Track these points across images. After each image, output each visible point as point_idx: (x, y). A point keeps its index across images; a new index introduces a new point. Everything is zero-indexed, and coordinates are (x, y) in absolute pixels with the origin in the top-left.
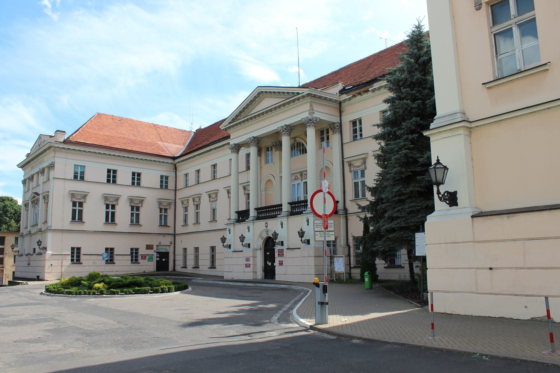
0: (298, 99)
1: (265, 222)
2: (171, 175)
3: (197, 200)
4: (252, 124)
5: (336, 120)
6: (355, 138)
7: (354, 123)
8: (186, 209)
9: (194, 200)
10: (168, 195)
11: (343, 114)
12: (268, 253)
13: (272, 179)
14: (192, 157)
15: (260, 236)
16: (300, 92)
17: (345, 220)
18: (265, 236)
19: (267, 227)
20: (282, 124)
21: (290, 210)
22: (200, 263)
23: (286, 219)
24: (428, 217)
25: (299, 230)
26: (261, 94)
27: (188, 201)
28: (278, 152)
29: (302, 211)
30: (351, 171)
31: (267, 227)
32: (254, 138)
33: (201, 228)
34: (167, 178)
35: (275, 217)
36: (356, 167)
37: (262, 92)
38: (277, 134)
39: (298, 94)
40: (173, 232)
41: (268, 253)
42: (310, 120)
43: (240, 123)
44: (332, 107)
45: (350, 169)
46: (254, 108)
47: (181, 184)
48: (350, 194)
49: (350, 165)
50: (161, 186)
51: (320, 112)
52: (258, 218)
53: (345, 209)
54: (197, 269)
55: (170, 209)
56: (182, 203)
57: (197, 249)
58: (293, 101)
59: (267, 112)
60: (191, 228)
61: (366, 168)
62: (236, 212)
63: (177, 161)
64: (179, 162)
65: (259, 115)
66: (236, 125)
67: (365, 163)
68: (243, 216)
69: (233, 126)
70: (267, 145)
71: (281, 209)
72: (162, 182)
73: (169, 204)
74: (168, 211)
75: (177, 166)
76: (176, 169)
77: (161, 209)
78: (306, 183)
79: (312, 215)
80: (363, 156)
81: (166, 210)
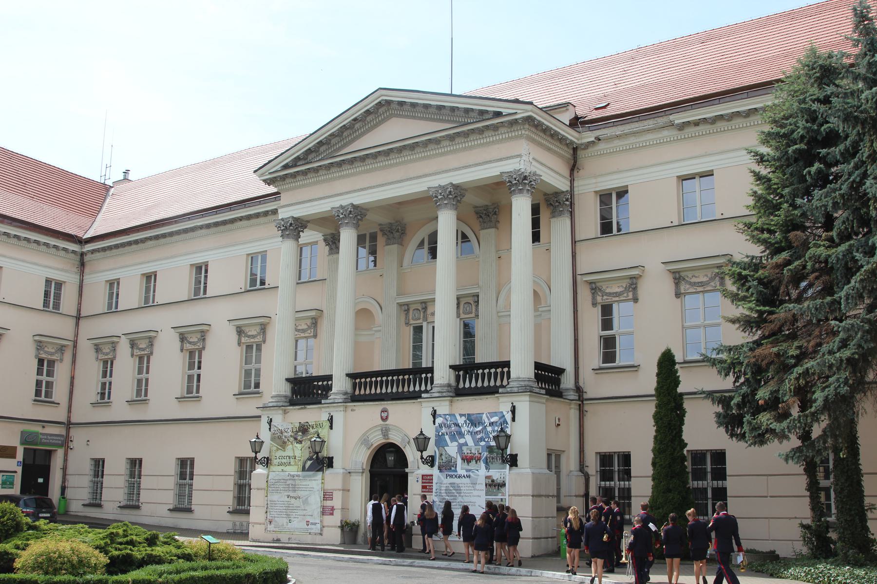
0: (495, 128)
1: (380, 408)
2: (70, 278)
5: (563, 185)
6: (606, 228)
7: (605, 198)
8: (107, 368)
9: (133, 344)
10: (58, 327)
12: (40, 480)
13: (375, 309)
15: (364, 441)
16: (505, 111)
18: (377, 440)
23: (447, 403)
24: (683, 437)
26: (383, 107)
27: (114, 346)
28: (394, 247)
29: (421, 392)
30: (594, 304)
33: (152, 412)
34: (59, 285)
35: (415, 396)
36: (610, 294)
37: (389, 103)
38: (428, 202)
39: (498, 114)
40: (63, 419)
41: (40, 480)
42: (525, 178)
45: (594, 298)
47: (96, 300)
48: (592, 355)
49: (594, 288)
50: (46, 304)
51: (542, 164)
53: (579, 390)
55: (61, 360)
56: (98, 349)
57: (135, 464)
60: (119, 409)
61: (264, 341)
62: (288, 380)
63: (88, 247)
64: (93, 252)
66: (305, 173)
67: (151, 345)
69: (294, 176)
71: (329, 388)
72: (47, 294)
73: (62, 349)
76: (82, 264)
77: (41, 362)
78: (433, 327)
79: (527, 398)
80: (313, 313)
81: (51, 363)
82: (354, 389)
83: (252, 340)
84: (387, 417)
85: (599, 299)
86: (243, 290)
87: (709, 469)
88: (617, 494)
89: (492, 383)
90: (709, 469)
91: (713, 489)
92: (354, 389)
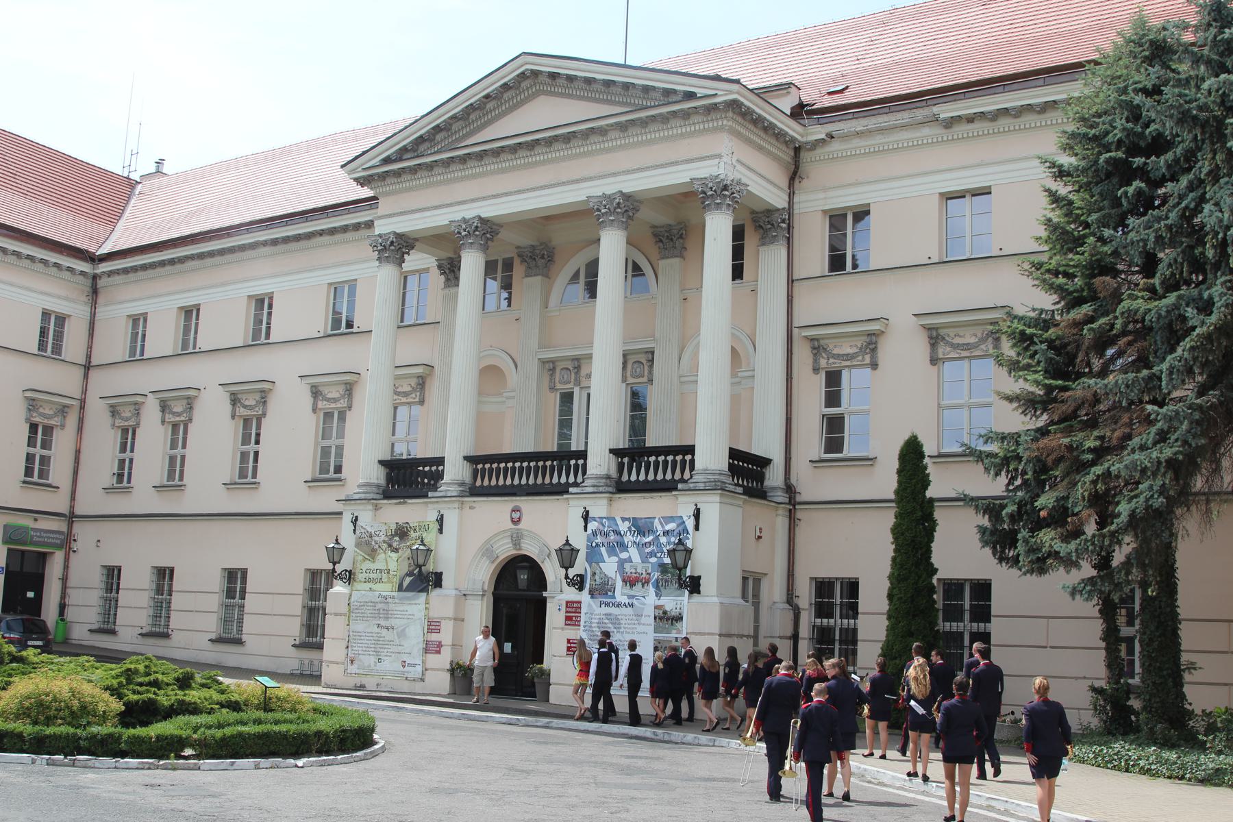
0: (686, 115)
1: (510, 506)
2: (76, 310)
3: (178, 409)
4: (513, 169)
5: (778, 200)
6: (837, 263)
7: (836, 220)
9: (164, 407)
10: (59, 379)
12: (30, 594)
13: (506, 365)
14: (172, 262)
15: (487, 551)
16: (700, 92)
18: (505, 551)
19: (516, 522)
20: (610, 187)
22: (123, 617)
23: (605, 502)
26: (529, 80)
27: (137, 408)
29: (568, 485)
30: (816, 370)
31: (516, 522)
32: (627, 197)
34: (61, 320)
35: (560, 490)
36: (838, 357)
37: (535, 74)
39: (690, 96)
40: (63, 508)
41: (30, 594)
42: (725, 188)
43: (430, 167)
44: (768, 153)
45: (816, 361)
49: (817, 347)
50: (42, 345)
51: (749, 168)
52: (475, 491)
53: (790, 489)
54: (162, 642)
55: (63, 426)
56: (114, 411)
57: (164, 575)
59: (550, 142)
60: (142, 498)
63: (104, 267)
64: (110, 274)
65: (497, 153)
66: (414, 170)
68: (408, 477)
70: (530, 255)
71: (440, 476)
72: (43, 332)
73: (63, 410)
74: (57, 434)
75: (101, 283)
77: (33, 428)
78: (589, 395)
79: (717, 499)
82: (475, 478)
83: (333, 405)
84: (519, 519)
86: (321, 334)
87: (967, 606)
88: (837, 637)
89: (669, 476)
90: (967, 606)
92: (475, 478)
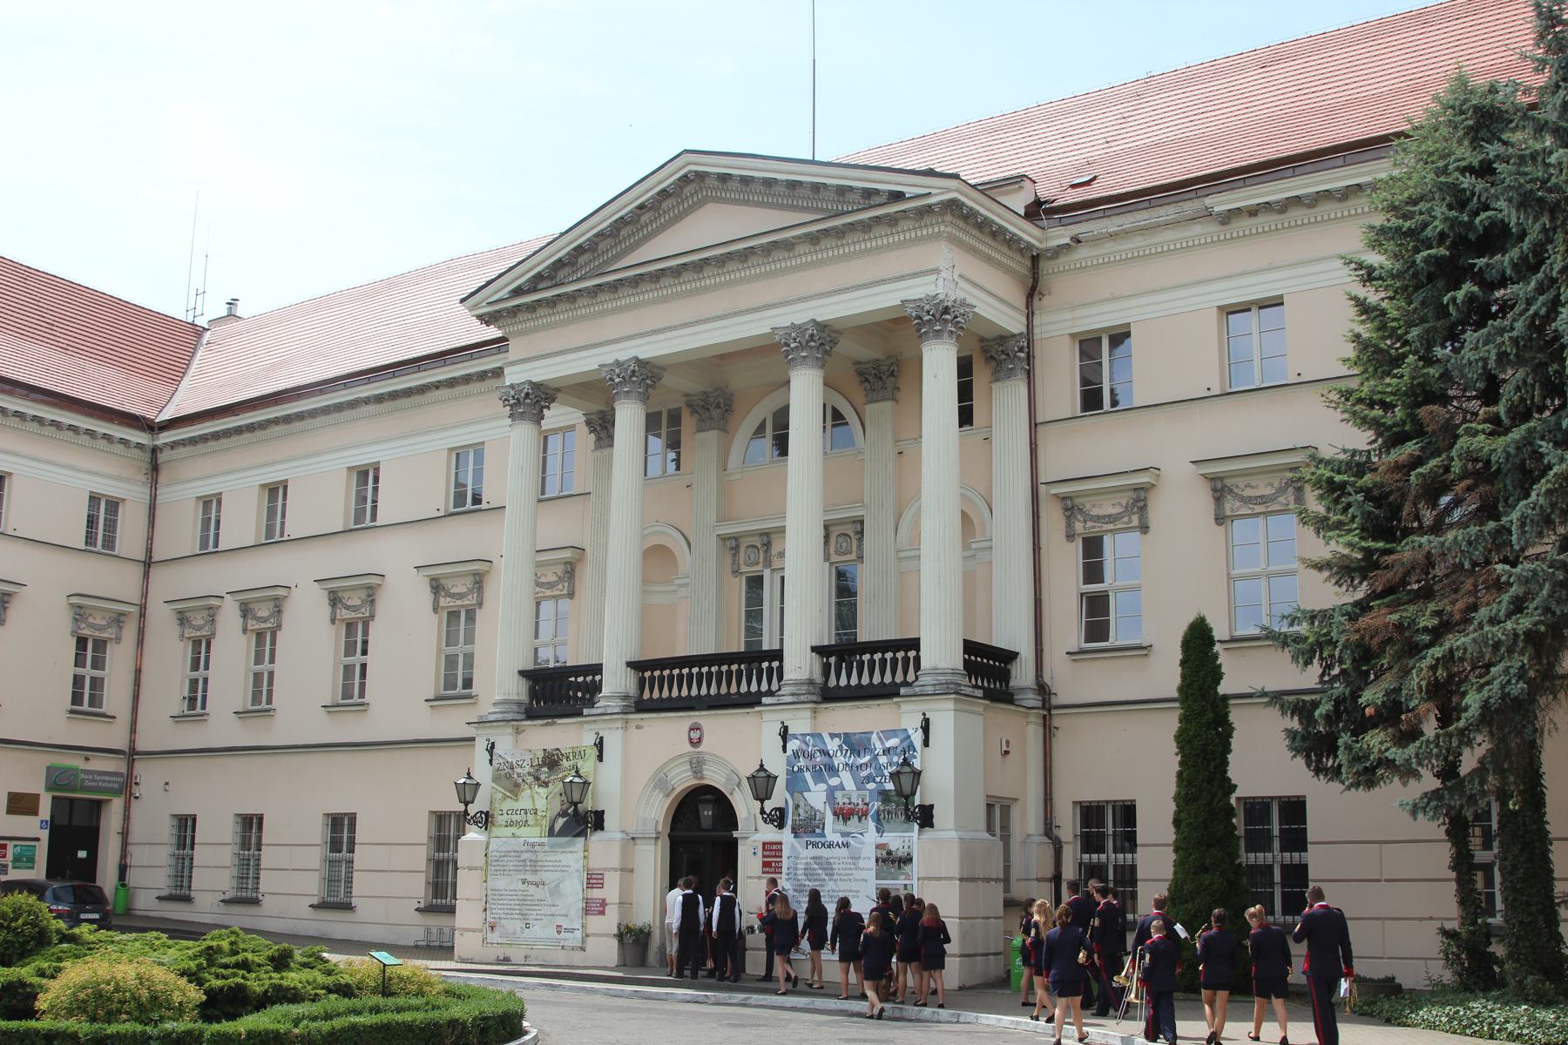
0: (892, 221)
1: (687, 724)
2: (132, 493)
3: (263, 613)
5: (1013, 323)
7: (1088, 346)
9: (246, 611)
10: (112, 580)
11: (163, 478)
12: (82, 854)
13: (677, 544)
14: (251, 428)
15: (660, 782)
16: (909, 191)
17: (1040, 730)
18: (683, 780)
20: (800, 315)
21: (632, 690)
23: (808, 714)
25: (752, 768)
27: (212, 614)
28: (712, 436)
29: (760, 694)
30: (1070, 537)
32: (822, 327)
33: (279, 731)
34: (114, 505)
35: (751, 701)
38: (773, 354)
39: (897, 196)
41: (82, 854)
42: (946, 310)
43: (572, 297)
45: (1069, 526)
46: (638, 244)
49: (1071, 507)
50: (90, 538)
51: (975, 285)
53: (1043, 689)
55: (118, 640)
56: (183, 619)
57: (251, 824)
58: (866, 227)
61: (480, 605)
64: (173, 445)
66: (551, 303)
68: (557, 691)
70: (702, 406)
71: (597, 687)
72: (91, 522)
73: (118, 619)
75: (162, 457)
77: (81, 642)
78: (783, 578)
79: (951, 705)
80: (567, 554)
81: (100, 645)
83: (459, 603)
84: (700, 740)
85: (1079, 527)
86: (442, 513)
87: (1276, 832)
89: (888, 679)
91: (1284, 867)
